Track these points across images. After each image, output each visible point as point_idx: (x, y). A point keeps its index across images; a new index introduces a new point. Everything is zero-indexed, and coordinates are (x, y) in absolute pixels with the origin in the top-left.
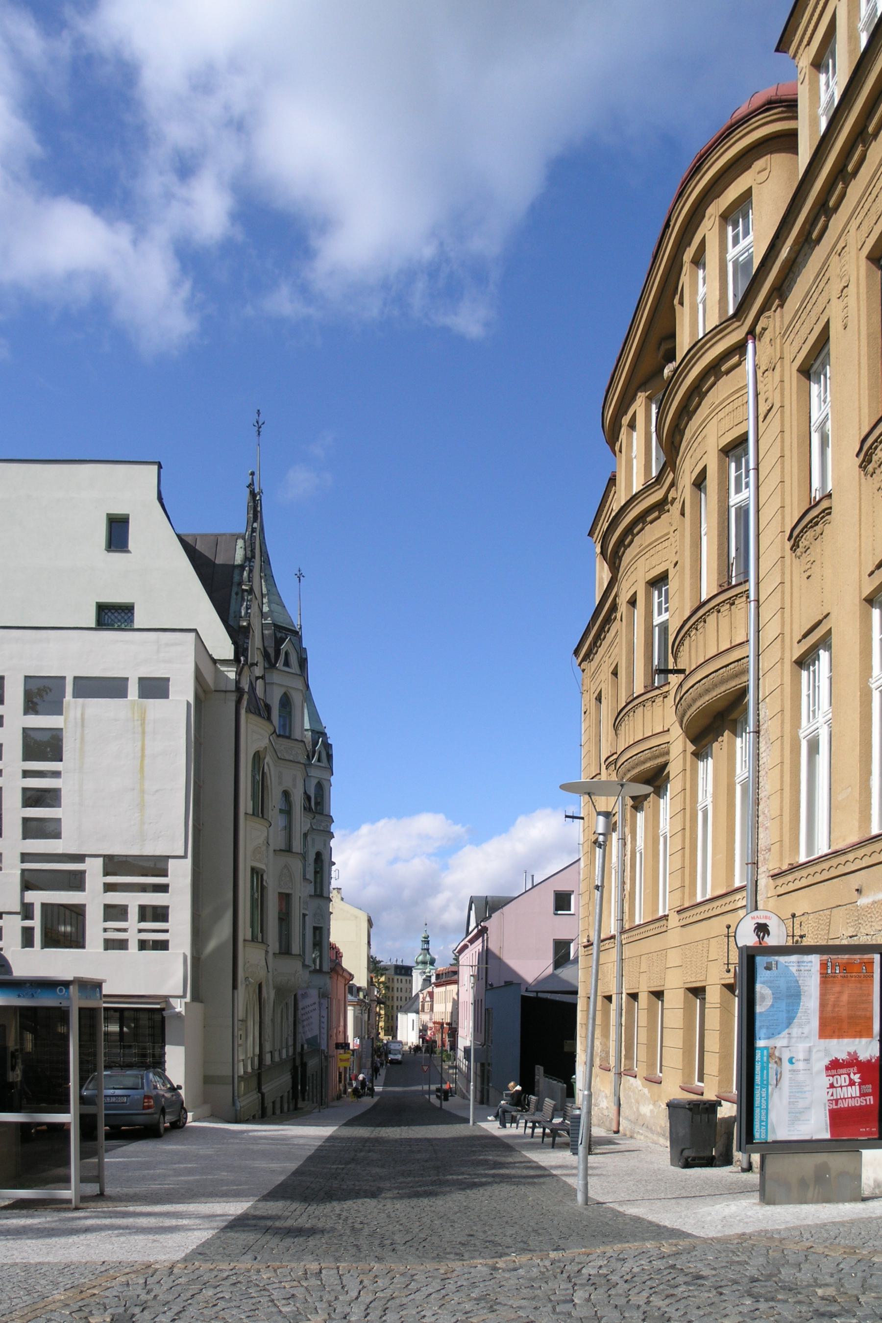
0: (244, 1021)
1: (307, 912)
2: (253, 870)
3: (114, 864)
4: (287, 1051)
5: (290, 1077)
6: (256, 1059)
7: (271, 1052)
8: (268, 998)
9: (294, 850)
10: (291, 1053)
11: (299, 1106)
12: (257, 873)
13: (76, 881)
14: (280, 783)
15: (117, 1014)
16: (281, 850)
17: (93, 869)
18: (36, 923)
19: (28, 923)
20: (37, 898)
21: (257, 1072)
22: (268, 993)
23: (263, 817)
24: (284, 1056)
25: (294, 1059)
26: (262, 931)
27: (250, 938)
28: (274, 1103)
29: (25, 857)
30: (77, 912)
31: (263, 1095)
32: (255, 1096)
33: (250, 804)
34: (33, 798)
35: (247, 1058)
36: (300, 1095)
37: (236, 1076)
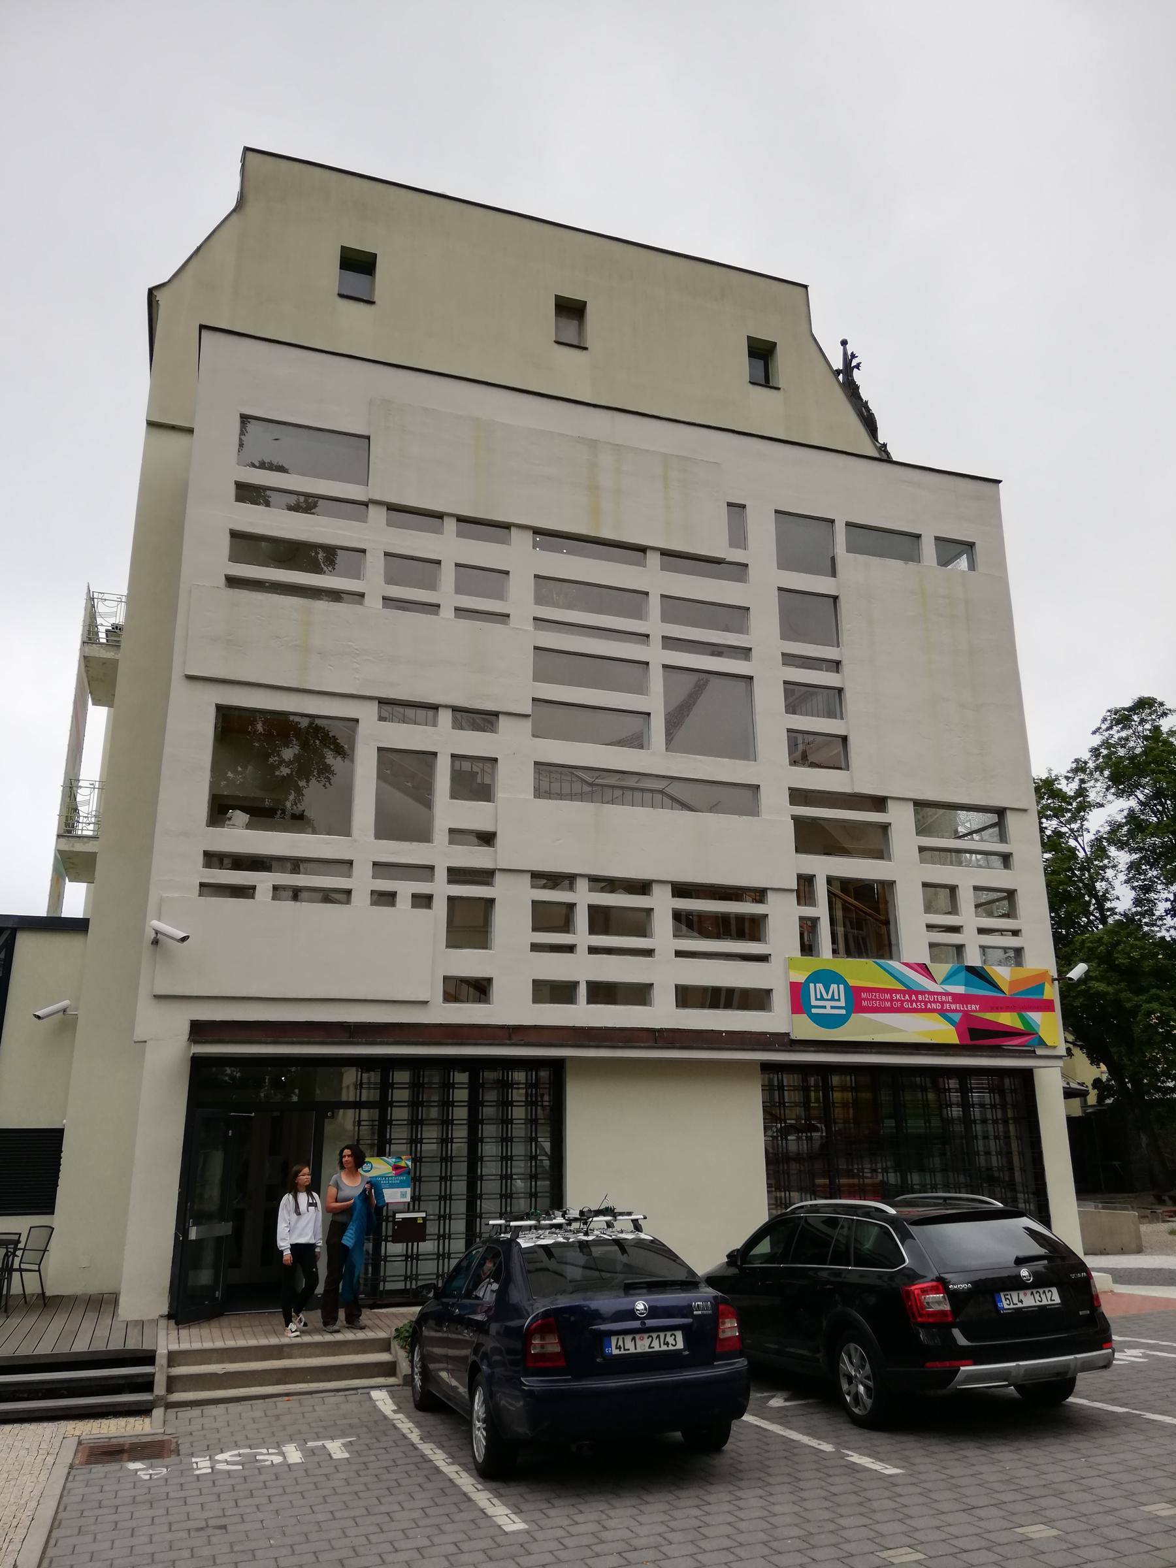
13: (876, 842)
18: (821, 910)
20: (823, 867)
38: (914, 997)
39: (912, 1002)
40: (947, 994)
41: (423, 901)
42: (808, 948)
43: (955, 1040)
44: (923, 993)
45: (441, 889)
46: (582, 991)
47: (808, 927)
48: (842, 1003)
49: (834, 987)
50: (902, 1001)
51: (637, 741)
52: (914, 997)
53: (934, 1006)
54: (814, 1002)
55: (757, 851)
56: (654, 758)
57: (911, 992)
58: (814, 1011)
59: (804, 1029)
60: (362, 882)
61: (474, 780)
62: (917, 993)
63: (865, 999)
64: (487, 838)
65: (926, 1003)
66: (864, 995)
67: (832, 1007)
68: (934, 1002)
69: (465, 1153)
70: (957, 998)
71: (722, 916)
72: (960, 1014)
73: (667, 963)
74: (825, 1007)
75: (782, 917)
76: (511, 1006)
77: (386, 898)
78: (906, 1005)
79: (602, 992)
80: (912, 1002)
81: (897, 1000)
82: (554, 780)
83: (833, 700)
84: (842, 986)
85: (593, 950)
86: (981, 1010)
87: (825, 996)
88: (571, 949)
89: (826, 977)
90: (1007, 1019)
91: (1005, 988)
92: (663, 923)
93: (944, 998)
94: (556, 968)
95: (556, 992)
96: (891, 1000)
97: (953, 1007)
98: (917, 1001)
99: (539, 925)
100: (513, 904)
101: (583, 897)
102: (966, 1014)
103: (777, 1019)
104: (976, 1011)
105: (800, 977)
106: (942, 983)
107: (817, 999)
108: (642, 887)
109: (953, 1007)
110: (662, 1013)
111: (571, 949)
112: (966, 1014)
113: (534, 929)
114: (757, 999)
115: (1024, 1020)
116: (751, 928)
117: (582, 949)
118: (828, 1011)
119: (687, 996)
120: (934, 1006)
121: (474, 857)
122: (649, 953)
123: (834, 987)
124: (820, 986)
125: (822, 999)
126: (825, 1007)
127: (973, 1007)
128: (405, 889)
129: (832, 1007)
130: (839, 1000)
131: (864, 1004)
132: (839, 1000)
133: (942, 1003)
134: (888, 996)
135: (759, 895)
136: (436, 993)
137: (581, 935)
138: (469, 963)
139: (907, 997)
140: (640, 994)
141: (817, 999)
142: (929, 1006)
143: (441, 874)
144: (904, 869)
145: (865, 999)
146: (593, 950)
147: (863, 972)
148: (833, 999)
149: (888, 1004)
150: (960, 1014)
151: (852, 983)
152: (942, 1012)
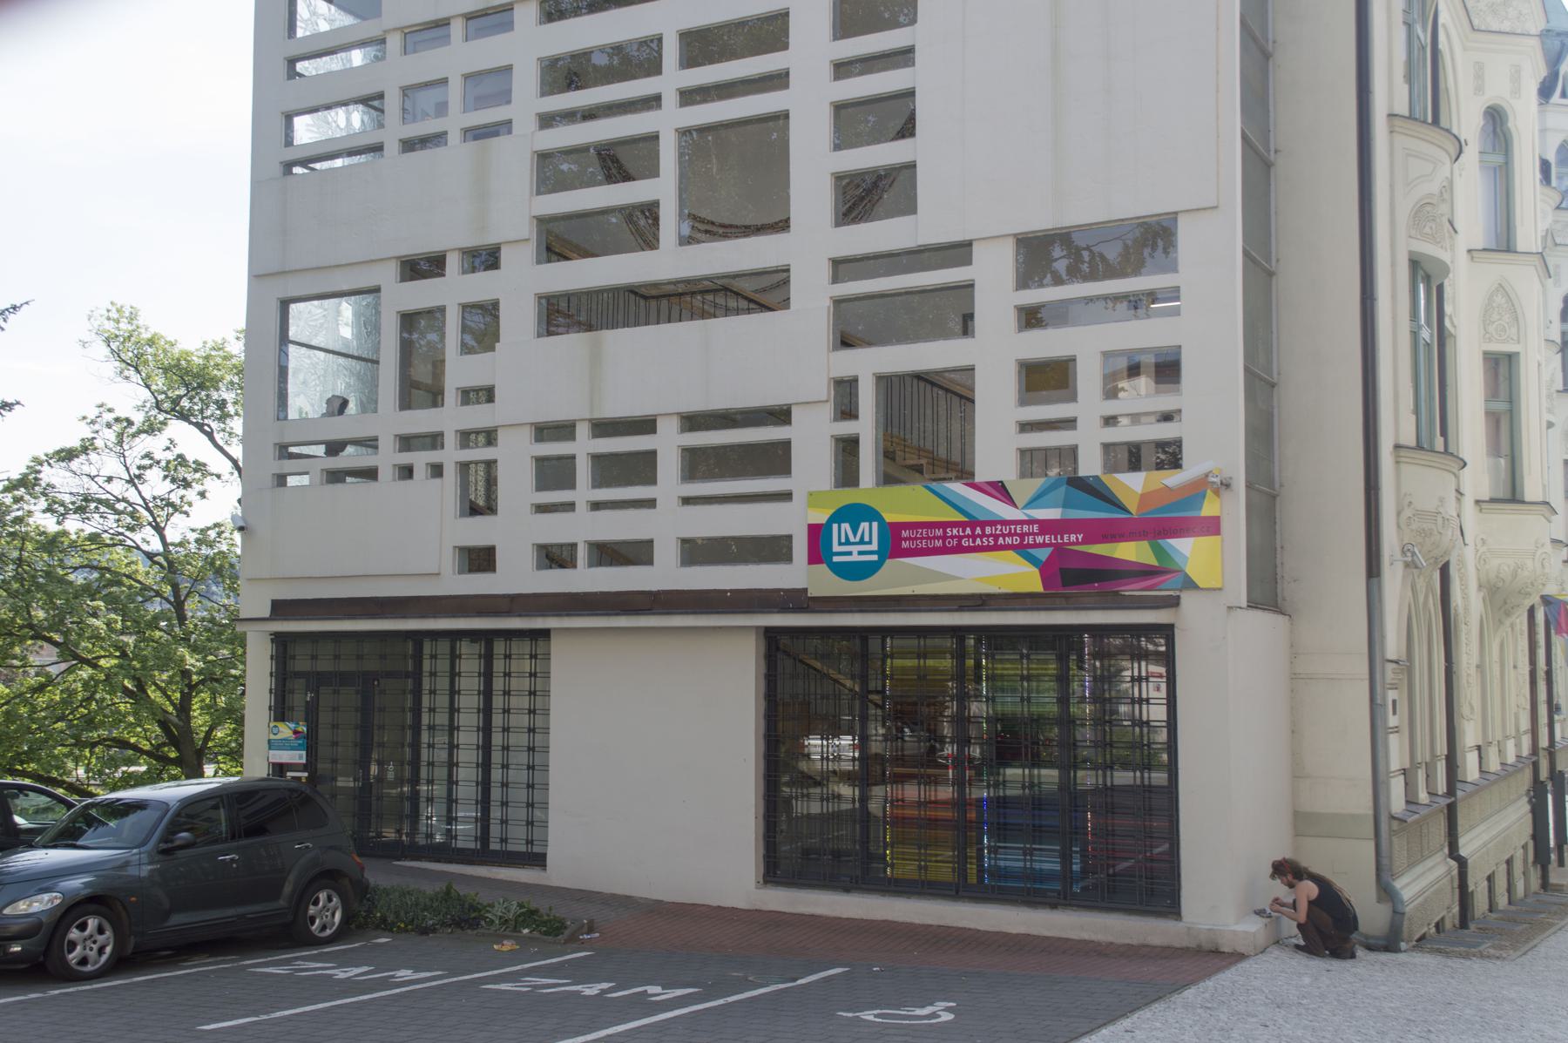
0: (1406, 666)
1: (1552, 419)
2: (1415, 264)
3: (1039, 254)
4: (1518, 745)
5: (1528, 807)
6: (1441, 768)
7: (1479, 748)
8: (1466, 609)
9: (1521, 245)
10: (1526, 751)
11: (1554, 879)
12: (1428, 279)
13: (955, 313)
14: (1479, 89)
15: (949, 643)
16: (1493, 500)
17: (994, 280)
18: (866, 427)
19: (846, 428)
20: (868, 364)
21: (1444, 802)
22: (1465, 597)
23: (1436, 121)
24: (1511, 759)
25: (1536, 766)
26: (1444, 433)
27: (1413, 443)
28: (1490, 879)
29: (842, 267)
30: (953, 391)
31: (1462, 863)
32: (1441, 870)
33: (1402, 90)
34: (853, 122)
35: (1415, 765)
36: (1553, 857)
37: (1384, 819)
38: (978, 531)
39: (974, 537)
40: (1031, 522)
41: (437, 470)
42: (847, 474)
43: (1036, 585)
44: (993, 523)
45: (451, 455)
46: (582, 554)
47: (848, 448)
48: (874, 546)
49: (864, 525)
50: (960, 538)
51: (648, 240)
52: (978, 531)
53: (1009, 540)
54: (836, 548)
55: (783, 359)
56: (671, 260)
57: (973, 524)
58: (836, 559)
59: (823, 582)
60: (387, 458)
61: (483, 324)
62: (983, 524)
63: (906, 539)
64: (488, 394)
65: (996, 537)
66: (905, 534)
67: (860, 553)
68: (1010, 535)
69: (494, 716)
70: (1046, 526)
71: (742, 448)
72: (1050, 550)
73: (670, 516)
74: (850, 553)
75: (813, 440)
76: (517, 574)
77: (407, 472)
78: (965, 543)
79: (608, 554)
80: (974, 537)
81: (952, 537)
82: (560, 314)
83: (897, 115)
84: (875, 524)
85: (596, 506)
86: (1085, 542)
87: (852, 539)
88: (569, 507)
89: (854, 514)
90: (1130, 551)
91: (1133, 506)
92: (669, 466)
93: (1025, 528)
94: (556, 530)
95: (554, 557)
96: (944, 538)
97: (1039, 539)
98: (983, 535)
99: (542, 484)
100: (515, 460)
101: (584, 446)
102: (1059, 550)
103: (795, 574)
104: (1078, 543)
105: (821, 517)
106: (1026, 507)
107: (840, 544)
108: (646, 425)
109: (1039, 539)
110: (666, 573)
111: (569, 507)
112: (1059, 550)
113: (653, 453)
114: (773, 549)
115: (1159, 552)
116: (776, 459)
117: (582, 507)
118: (855, 558)
119: (696, 551)
120: (1009, 540)
121: (478, 417)
122: (650, 503)
123: (864, 525)
124: (846, 526)
125: (848, 542)
126: (850, 553)
127: (1073, 538)
128: (420, 459)
129: (860, 553)
130: (870, 543)
131: (905, 545)
132: (870, 543)
133: (1022, 536)
134: (939, 532)
135: (781, 415)
136: (448, 562)
137: (584, 491)
138: (477, 532)
139: (968, 531)
140: (635, 553)
141: (840, 544)
142: (1001, 541)
143: (450, 440)
144: (992, 354)
145: (906, 539)
146: (596, 506)
147: (911, 504)
148: (862, 542)
149: (939, 543)
150: (1050, 550)
151: (889, 518)
152: (1020, 548)
